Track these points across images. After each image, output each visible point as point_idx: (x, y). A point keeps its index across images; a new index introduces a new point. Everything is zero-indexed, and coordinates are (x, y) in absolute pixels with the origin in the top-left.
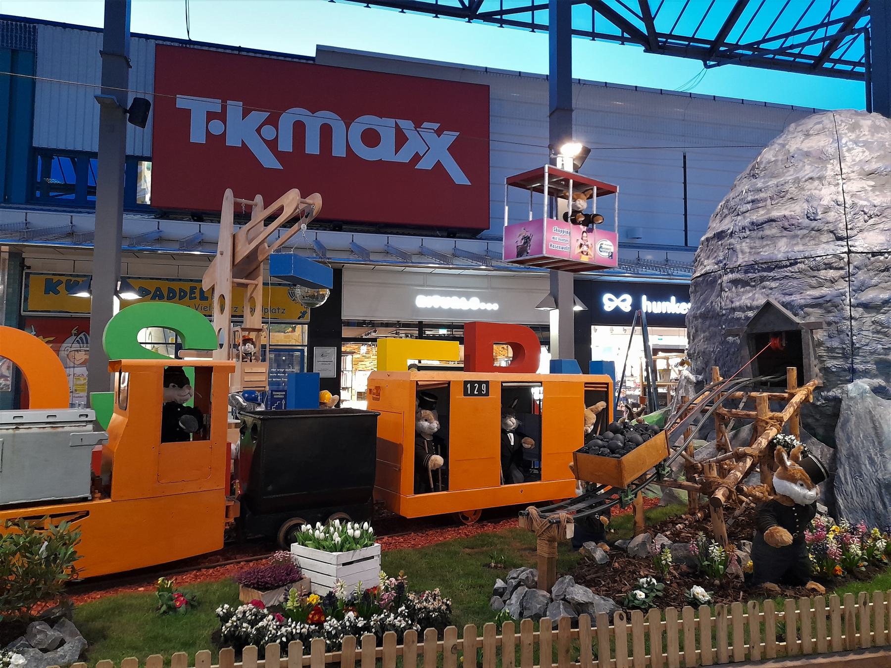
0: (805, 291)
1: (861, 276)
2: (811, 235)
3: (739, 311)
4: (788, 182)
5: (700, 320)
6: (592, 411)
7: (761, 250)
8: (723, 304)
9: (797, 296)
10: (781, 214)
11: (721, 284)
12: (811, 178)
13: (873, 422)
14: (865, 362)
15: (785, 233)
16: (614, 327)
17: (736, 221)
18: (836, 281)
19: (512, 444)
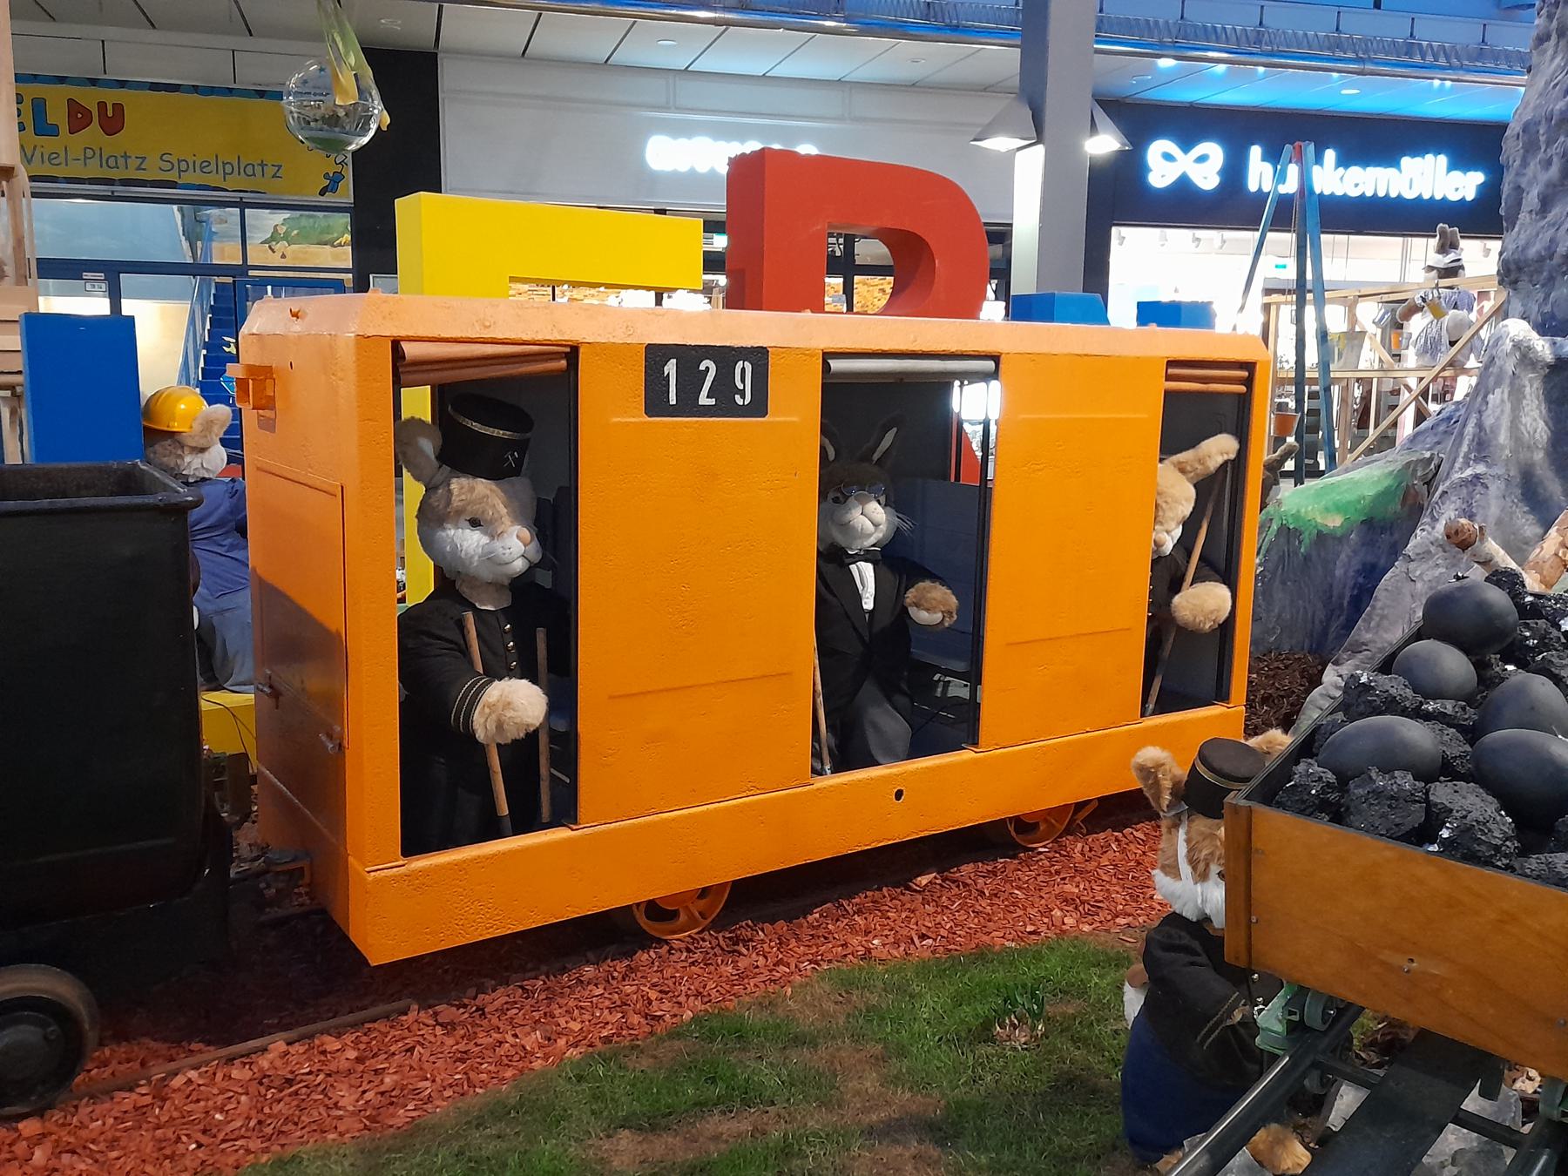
6: (1182, 471)
19: (868, 604)
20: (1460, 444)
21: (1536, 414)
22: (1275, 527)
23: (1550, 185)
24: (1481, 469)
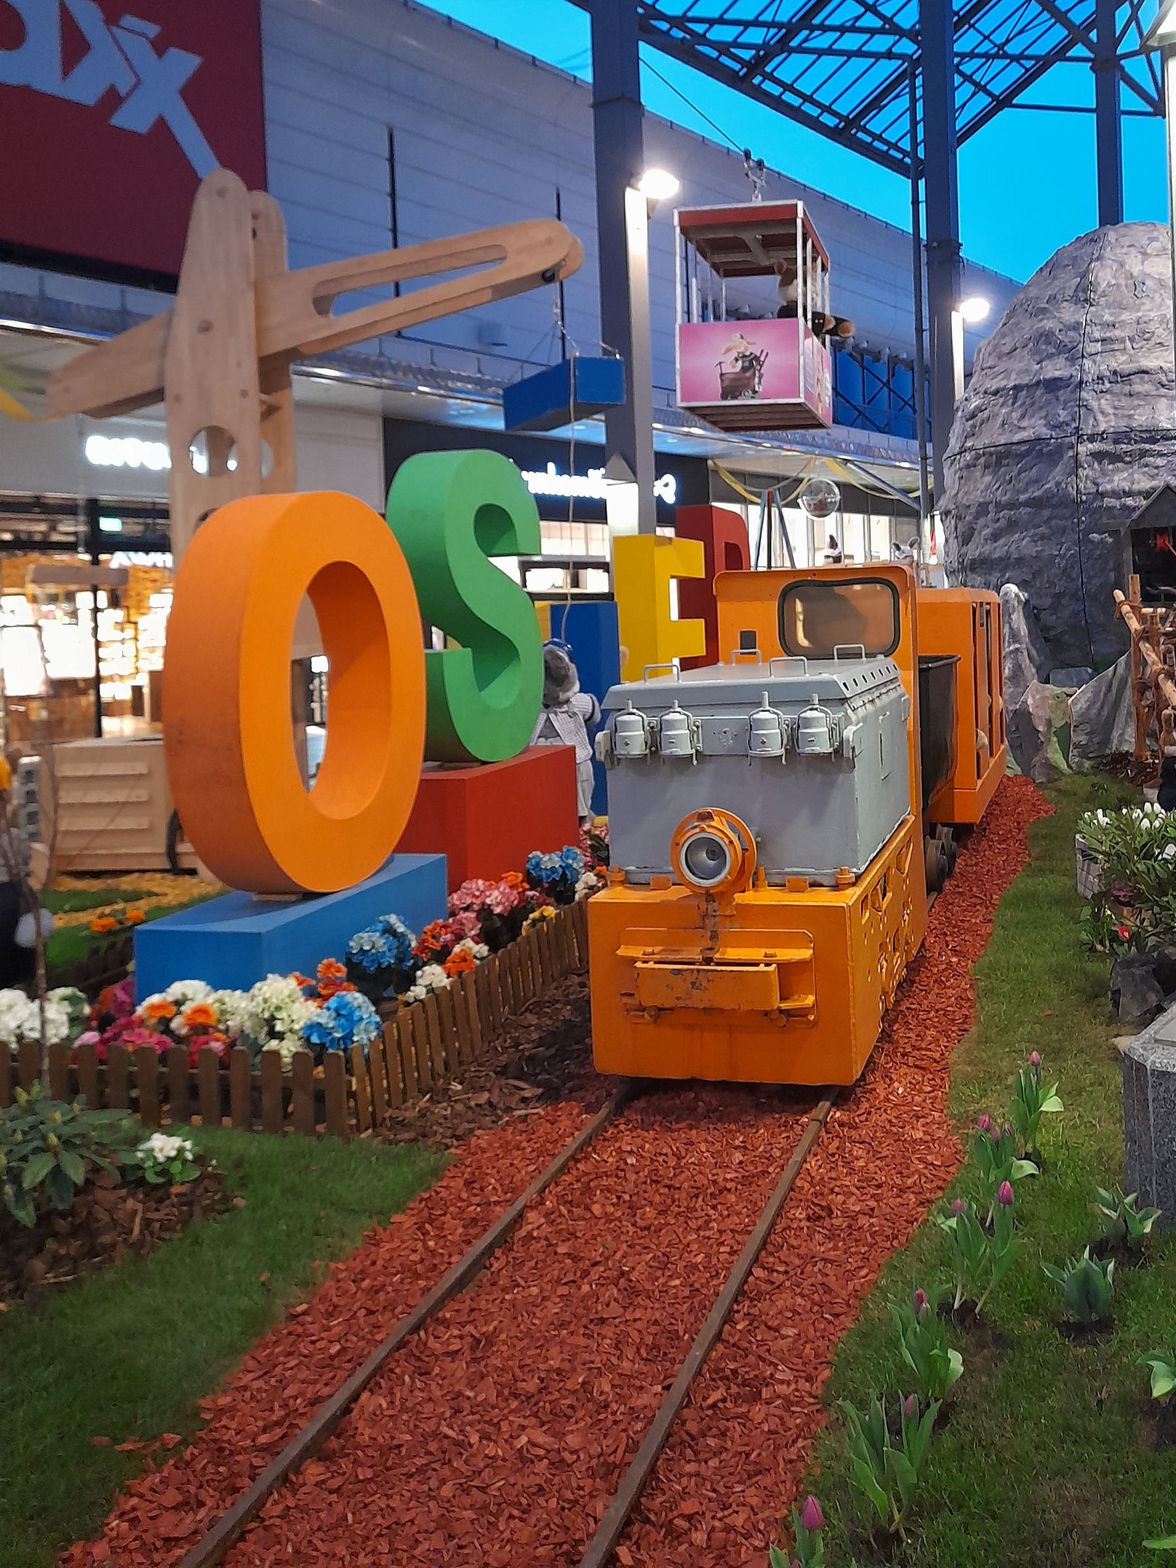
8: (1082, 485)
15: (1163, 391)
24: (1017, 646)
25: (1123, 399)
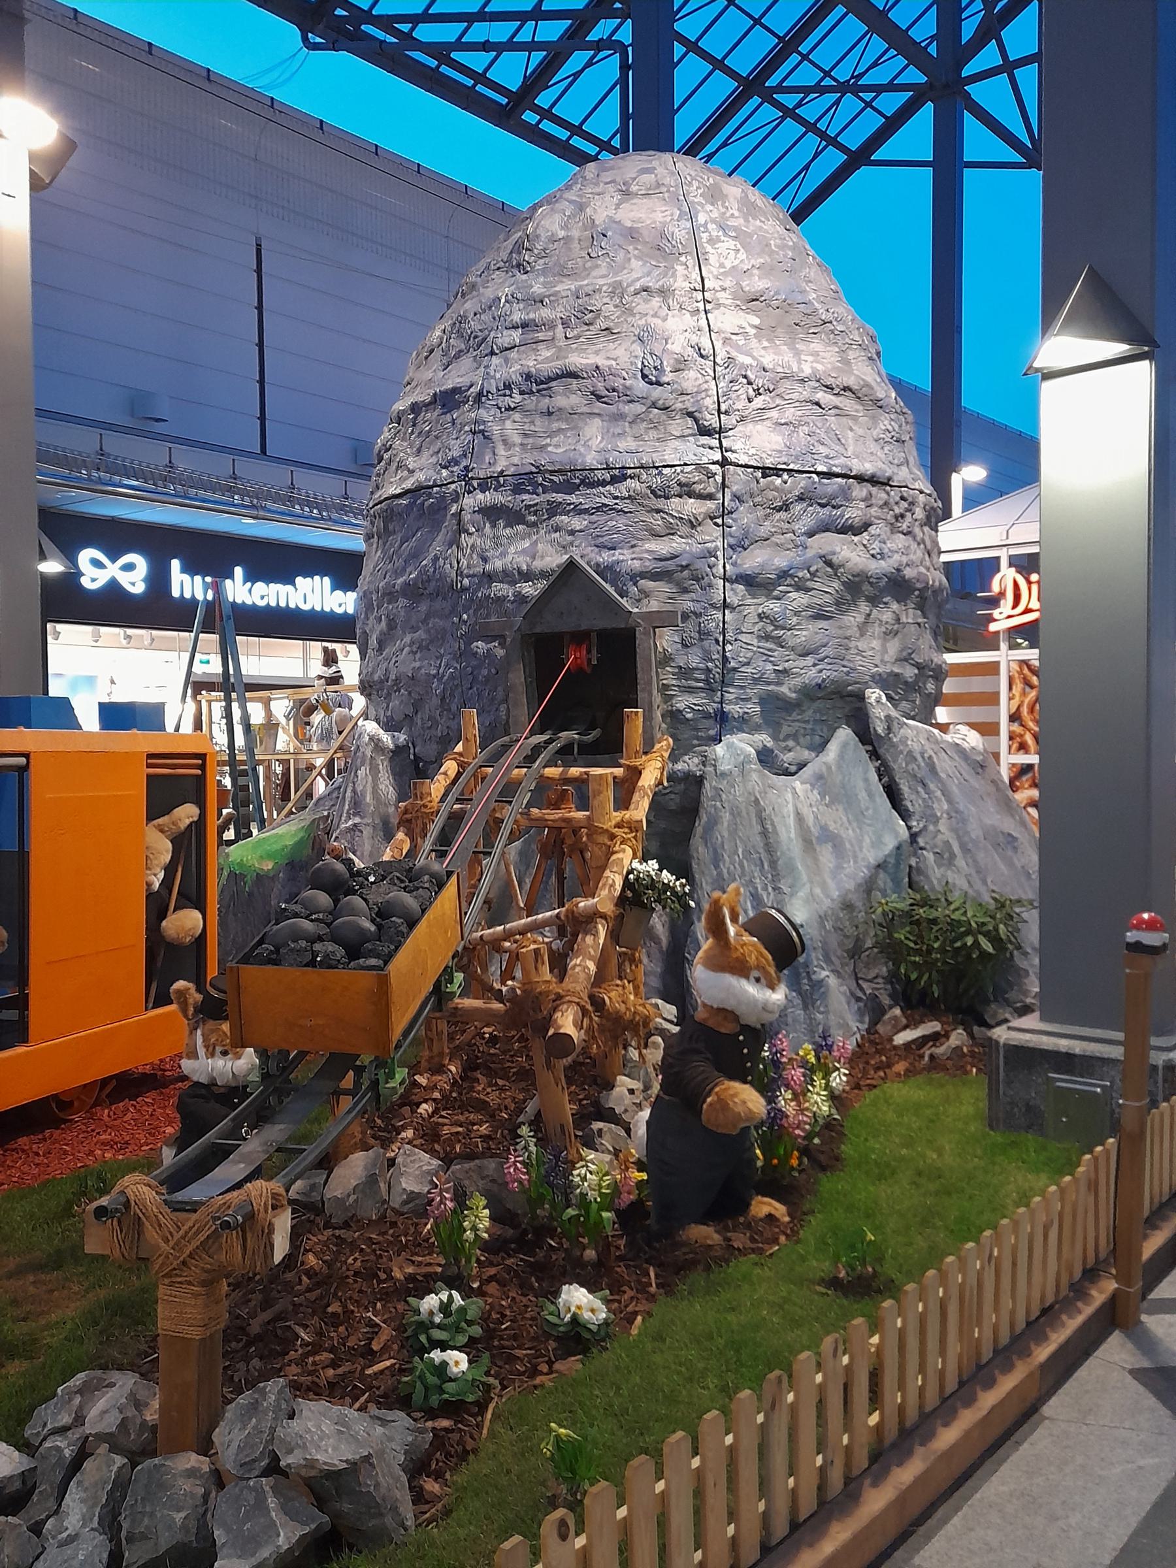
0: (640, 543)
1: (745, 517)
2: (651, 416)
3: (500, 582)
4: (600, 290)
5: (402, 602)
6: (162, 831)
7: (548, 440)
9: (625, 552)
10: (589, 361)
11: (459, 514)
12: (645, 290)
13: (762, 821)
14: (743, 700)
15: (599, 407)
16: (104, 630)
17: (486, 367)
18: (699, 525)
20: (344, 805)
21: (387, 782)
22: (225, 873)
23: (382, 633)
24: (357, 820)
25: (538, 421)
